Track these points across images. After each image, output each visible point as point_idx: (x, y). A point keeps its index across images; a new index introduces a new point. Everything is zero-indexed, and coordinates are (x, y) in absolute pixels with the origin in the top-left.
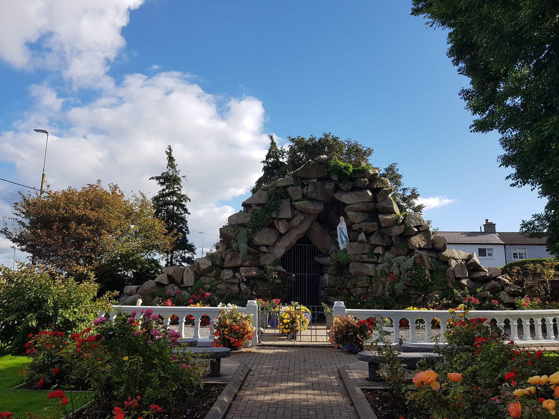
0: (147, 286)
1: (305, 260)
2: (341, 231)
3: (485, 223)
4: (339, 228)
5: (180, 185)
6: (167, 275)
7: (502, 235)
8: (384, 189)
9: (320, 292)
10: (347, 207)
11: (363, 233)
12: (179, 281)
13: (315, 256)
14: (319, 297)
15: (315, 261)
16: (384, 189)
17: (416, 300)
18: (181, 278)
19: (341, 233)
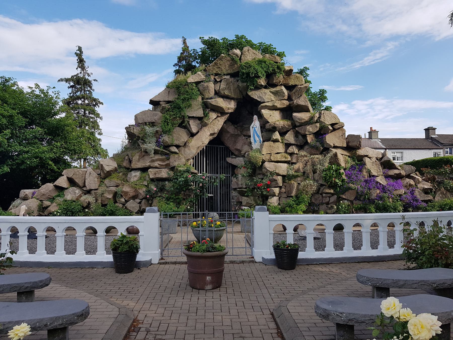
0: (44, 190)
1: (217, 162)
2: (254, 130)
3: (369, 131)
4: (253, 128)
5: (91, 87)
6: (67, 177)
7: (383, 140)
8: (298, 87)
9: (232, 193)
10: (262, 105)
11: (277, 132)
12: (81, 184)
13: (227, 157)
14: (231, 198)
15: (227, 162)
16: (298, 87)
17: (329, 199)
18: (83, 181)
19: (254, 132)
